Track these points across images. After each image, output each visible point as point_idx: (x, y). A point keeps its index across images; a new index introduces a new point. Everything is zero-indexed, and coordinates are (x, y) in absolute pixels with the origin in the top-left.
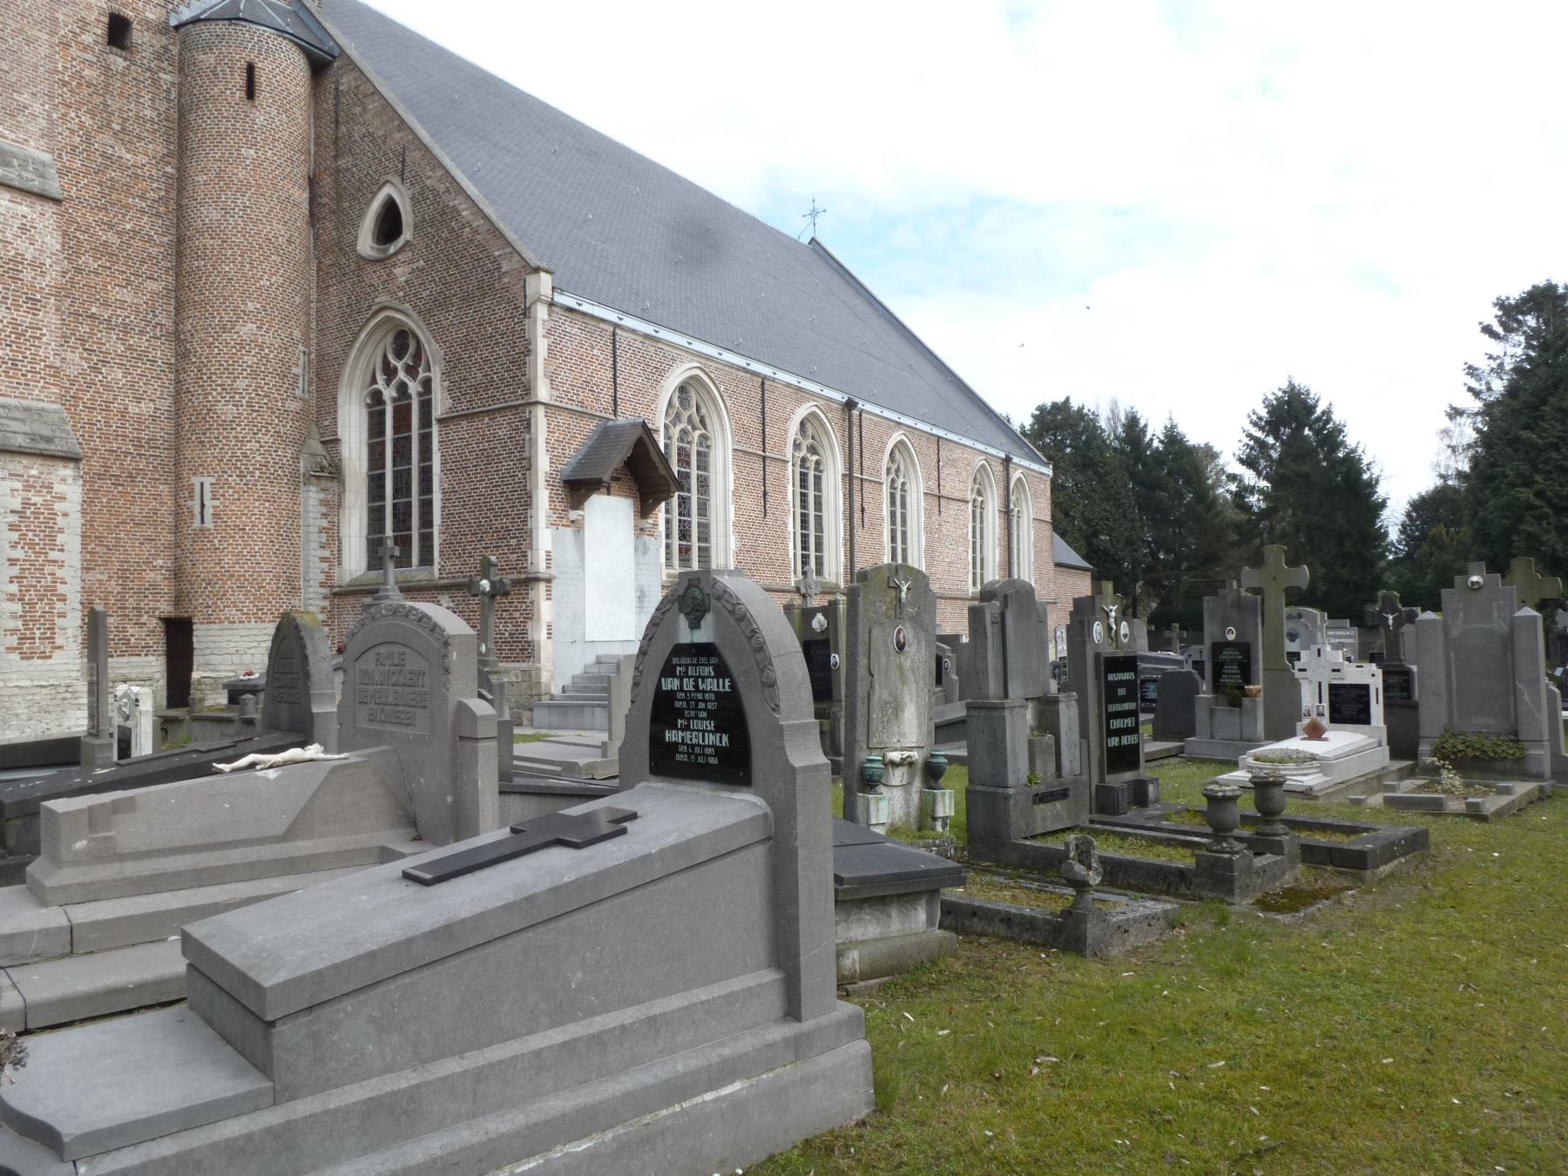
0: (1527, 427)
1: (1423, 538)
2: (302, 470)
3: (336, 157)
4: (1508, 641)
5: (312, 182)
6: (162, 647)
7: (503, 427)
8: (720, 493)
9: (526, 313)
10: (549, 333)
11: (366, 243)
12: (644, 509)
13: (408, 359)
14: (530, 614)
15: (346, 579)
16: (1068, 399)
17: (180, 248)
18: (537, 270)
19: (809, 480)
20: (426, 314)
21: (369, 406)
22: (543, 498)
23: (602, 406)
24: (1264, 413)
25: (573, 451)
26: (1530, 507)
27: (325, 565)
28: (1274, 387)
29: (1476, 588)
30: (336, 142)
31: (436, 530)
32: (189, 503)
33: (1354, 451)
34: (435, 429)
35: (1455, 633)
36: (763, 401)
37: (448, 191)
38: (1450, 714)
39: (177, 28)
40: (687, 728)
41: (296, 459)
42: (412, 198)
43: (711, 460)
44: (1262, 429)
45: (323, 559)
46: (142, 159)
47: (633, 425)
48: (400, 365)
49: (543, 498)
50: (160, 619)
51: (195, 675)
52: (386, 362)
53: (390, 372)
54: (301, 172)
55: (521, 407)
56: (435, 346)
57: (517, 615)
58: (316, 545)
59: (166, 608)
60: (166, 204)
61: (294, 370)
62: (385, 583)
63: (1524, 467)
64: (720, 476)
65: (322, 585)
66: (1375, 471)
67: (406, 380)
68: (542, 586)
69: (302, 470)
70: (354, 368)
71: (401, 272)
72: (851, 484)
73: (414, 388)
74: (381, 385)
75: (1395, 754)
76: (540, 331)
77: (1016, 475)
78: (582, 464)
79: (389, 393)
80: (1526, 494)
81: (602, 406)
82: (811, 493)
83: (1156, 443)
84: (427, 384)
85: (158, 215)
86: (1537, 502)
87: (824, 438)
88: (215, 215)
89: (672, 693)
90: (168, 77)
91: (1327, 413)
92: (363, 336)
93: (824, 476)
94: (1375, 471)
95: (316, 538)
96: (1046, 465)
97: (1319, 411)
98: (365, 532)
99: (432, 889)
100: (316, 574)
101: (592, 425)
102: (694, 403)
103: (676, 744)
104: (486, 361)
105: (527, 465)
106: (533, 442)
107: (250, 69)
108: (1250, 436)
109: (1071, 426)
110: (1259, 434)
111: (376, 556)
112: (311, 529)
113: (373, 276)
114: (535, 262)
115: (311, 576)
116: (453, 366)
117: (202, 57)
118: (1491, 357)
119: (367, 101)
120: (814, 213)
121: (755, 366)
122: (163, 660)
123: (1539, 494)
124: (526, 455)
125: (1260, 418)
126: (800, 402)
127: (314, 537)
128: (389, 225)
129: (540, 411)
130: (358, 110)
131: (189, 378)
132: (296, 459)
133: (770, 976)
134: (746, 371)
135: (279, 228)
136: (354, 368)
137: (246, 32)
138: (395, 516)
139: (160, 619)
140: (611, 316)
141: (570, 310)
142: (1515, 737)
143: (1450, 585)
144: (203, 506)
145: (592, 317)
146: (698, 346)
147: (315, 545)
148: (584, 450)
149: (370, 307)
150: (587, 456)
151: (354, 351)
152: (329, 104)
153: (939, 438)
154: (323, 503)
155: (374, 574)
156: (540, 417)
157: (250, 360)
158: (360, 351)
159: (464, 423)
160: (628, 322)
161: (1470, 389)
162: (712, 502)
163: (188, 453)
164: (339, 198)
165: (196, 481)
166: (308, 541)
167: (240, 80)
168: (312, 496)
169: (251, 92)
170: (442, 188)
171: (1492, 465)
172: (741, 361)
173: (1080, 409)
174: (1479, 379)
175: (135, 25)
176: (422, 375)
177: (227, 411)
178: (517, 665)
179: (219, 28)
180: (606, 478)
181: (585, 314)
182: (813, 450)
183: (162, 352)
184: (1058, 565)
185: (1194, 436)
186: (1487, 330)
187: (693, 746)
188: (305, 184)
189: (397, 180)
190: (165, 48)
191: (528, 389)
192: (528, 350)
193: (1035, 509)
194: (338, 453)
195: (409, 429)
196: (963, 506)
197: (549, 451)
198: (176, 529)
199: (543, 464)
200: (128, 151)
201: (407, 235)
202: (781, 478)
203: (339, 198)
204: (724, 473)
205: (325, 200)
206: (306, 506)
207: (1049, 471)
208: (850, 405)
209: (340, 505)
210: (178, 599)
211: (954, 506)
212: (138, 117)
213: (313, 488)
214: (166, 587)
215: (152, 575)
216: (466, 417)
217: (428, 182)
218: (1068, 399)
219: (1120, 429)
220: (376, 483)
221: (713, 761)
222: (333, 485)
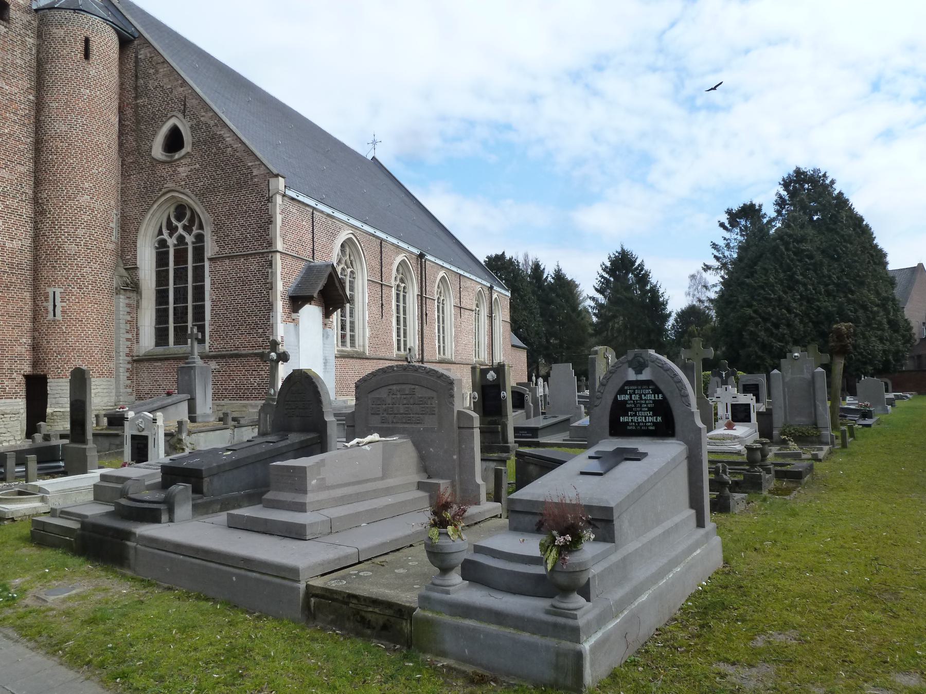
0: (747, 277)
1: (684, 332)
3: (136, 98)
4: (812, 382)
5: (121, 110)
6: (23, 393)
7: (254, 264)
8: (361, 304)
9: (270, 199)
10: (282, 212)
11: (158, 151)
12: (327, 315)
13: (185, 222)
15: (142, 352)
16: (504, 253)
17: (38, 146)
18: (277, 176)
19: (401, 297)
20: (201, 195)
21: (157, 248)
22: (280, 306)
23: (306, 255)
24: (608, 264)
26: (751, 318)
28: (614, 250)
29: (796, 359)
30: (136, 88)
31: (207, 323)
32: (45, 304)
33: (655, 286)
34: (207, 264)
35: (787, 379)
36: (381, 252)
37: (216, 125)
38: (786, 417)
39: (36, 11)
40: (635, 415)
42: (191, 127)
43: (356, 286)
44: (607, 273)
45: (128, 340)
46: (15, 90)
47: (327, 266)
48: (180, 225)
49: (280, 306)
50: (24, 375)
51: (49, 410)
52: (169, 222)
53: (172, 229)
54: (115, 104)
55: (264, 252)
56: (207, 215)
57: (263, 373)
58: (124, 331)
59: (27, 369)
60: (29, 118)
61: (111, 225)
62: (192, 353)
63: (748, 298)
64: (360, 295)
65: (127, 355)
66: (666, 297)
67: (184, 234)
70: (148, 225)
71: (183, 171)
72: (422, 300)
73: (189, 239)
74: (165, 235)
75: (762, 435)
76: (278, 211)
77: (495, 296)
78: (300, 285)
79: (171, 242)
80: (749, 311)
81: (306, 255)
82: (401, 305)
83: (549, 279)
84: (200, 238)
85: (24, 125)
86: (754, 315)
87: (408, 274)
88: (64, 128)
89: (625, 402)
90: (31, 40)
91: (641, 265)
92: (155, 206)
93: (407, 295)
94: (666, 297)
95: (124, 327)
96: (507, 290)
97: (637, 264)
99: (606, 476)
100: (123, 350)
101: (303, 265)
102: (347, 253)
103: (627, 423)
104: (242, 226)
105: (270, 287)
106: (274, 274)
107: (87, 41)
108: (602, 277)
109: (506, 268)
110: (606, 276)
111: (161, 336)
113: (163, 171)
114: (275, 172)
116: (218, 228)
117: (55, 30)
118: (725, 239)
119: (159, 66)
120: (374, 143)
121: (379, 234)
122: (24, 401)
123: (755, 312)
125: (606, 267)
126: (398, 254)
127: (123, 326)
128: (174, 141)
129: (278, 255)
130: (152, 71)
131: (45, 227)
133: (693, 512)
134: (374, 236)
135: (103, 139)
136: (148, 225)
137: (84, 18)
138: (175, 314)
139: (24, 375)
140: (312, 203)
141: (293, 199)
142: (815, 425)
143: (785, 357)
144: (55, 306)
145: (303, 203)
146: (353, 221)
148: (299, 279)
149: (160, 190)
150: (300, 283)
151: (149, 216)
152: (131, 65)
153: (461, 275)
154: (129, 305)
155: (160, 349)
156: (278, 260)
157: (86, 218)
158: (153, 215)
159: (227, 261)
160: (321, 207)
161: (715, 257)
162: (356, 309)
163: (44, 273)
164: (138, 122)
165: (53, 289)
167: (80, 47)
168: (122, 300)
169: (87, 55)
170: (212, 123)
171: (731, 296)
172: (371, 230)
173: (511, 259)
174: (718, 251)
175: (11, 6)
176: (195, 231)
177: (71, 248)
179: (68, 14)
180: (315, 295)
181: (299, 202)
182: (402, 281)
183: (26, 210)
184: (513, 346)
185: (570, 274)
186: (722, 225)
187: (639, 423)
188: (116, 111)
189: (180, 116)
190: (29, 22)
191: (270, 244)
192: (270, 221)
193: (503, 315)
195: (186, 262)
196: (471, 313)
197: (284, 279)
198: (35, 319)
199: (280, 286)
200: (7, 84)
201: (187, 148)
202: (389, 296)
203: (138, 122)
204: (362, 292)
205: (127, 123)
207: (509, 294)
208: (421, 256)
209: (138, 307)
210: (35, 364)
211: (467, 312)
212: (13, 64)
213: (122, 297)
214: (28, 356)
215: (19, 348)
216: (228, 257)
217: (202, 119)
218: (504, 253)
219: (529, 271)
220: (162, 297)
221: (651, 428)
222: (133, 295)
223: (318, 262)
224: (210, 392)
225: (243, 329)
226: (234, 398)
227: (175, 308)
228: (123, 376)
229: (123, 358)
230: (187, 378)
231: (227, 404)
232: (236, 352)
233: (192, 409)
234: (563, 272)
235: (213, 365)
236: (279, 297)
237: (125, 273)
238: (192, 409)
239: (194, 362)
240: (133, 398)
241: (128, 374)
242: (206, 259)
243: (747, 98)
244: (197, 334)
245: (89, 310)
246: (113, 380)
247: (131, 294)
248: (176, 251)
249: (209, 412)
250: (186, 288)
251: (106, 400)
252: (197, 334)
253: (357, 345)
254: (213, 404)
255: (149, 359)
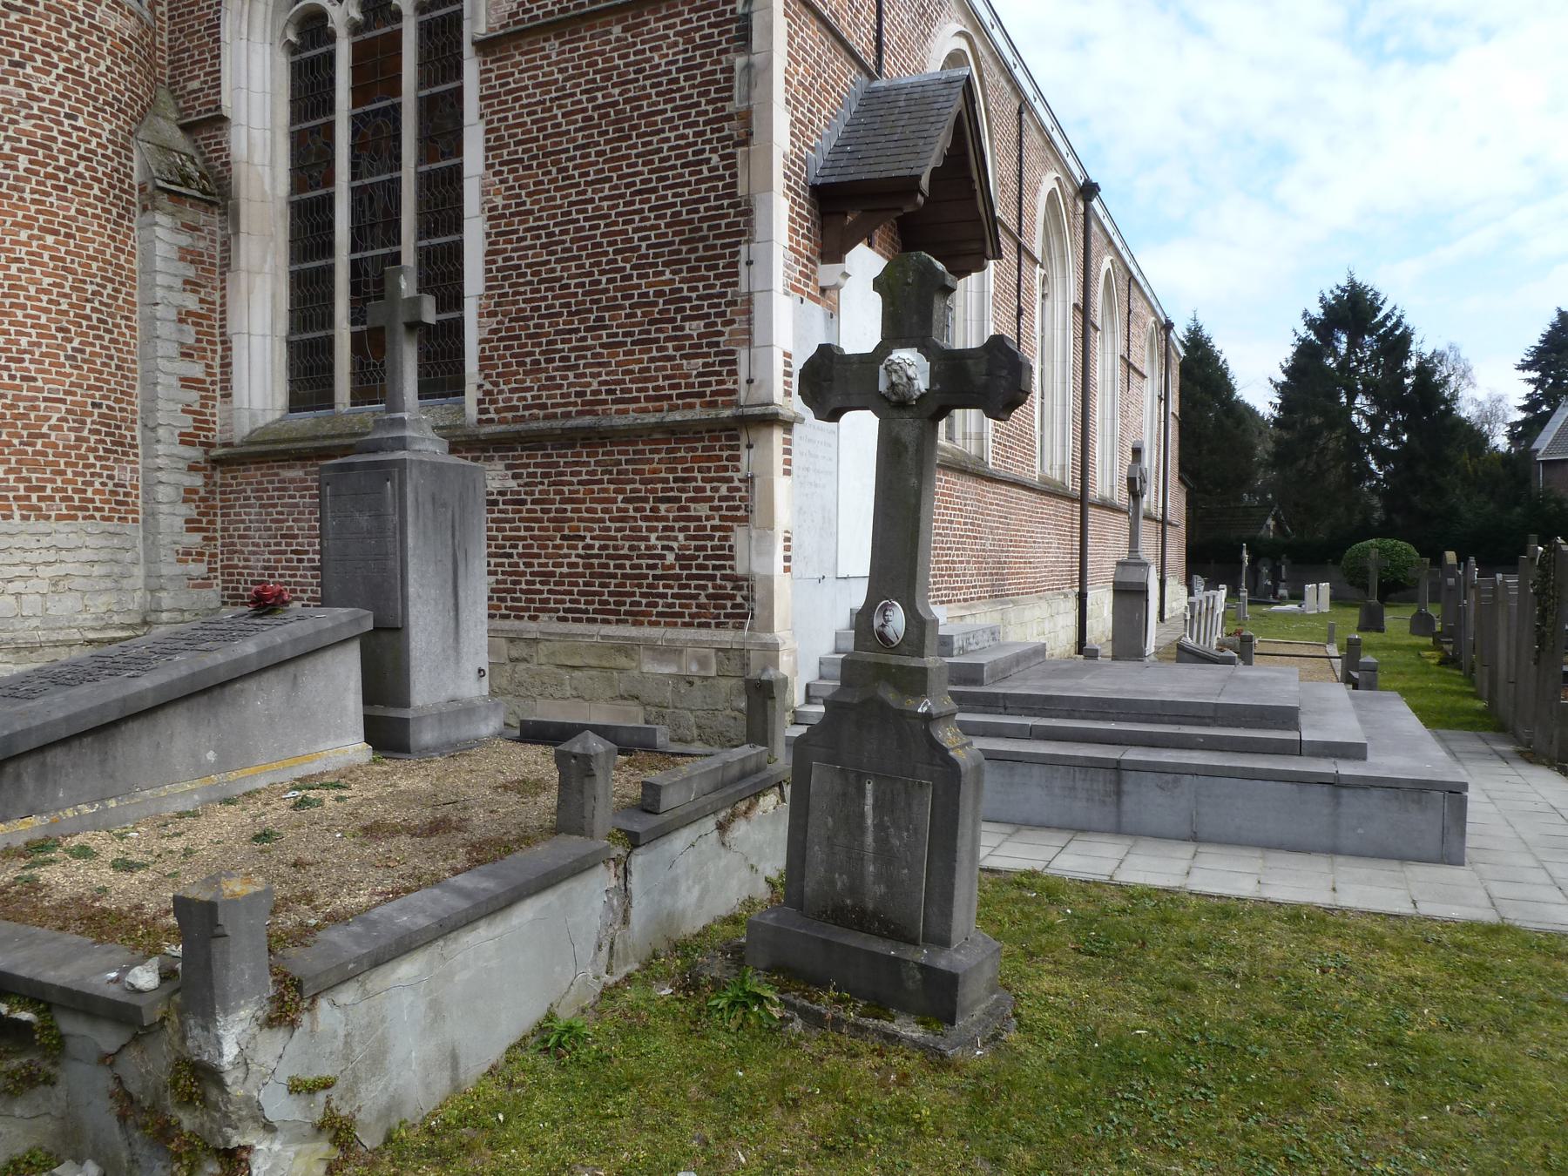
2: (137, 178)
14: (744, 506)
15: (243, 428)
21: (293, 49)
22: (781, 219)
25: (827, 132)
27: (193, 396)
28: (1331, 282)
41: (124, 149)
45: (188, 383)
49: (781, 219)
57: (702, 510)
58: (174, 350)
65: (186, 440)
68: (778, 435)
69: (137, 178)
97: (1381, 315)
98: (283, 326)
100: (172, 413)
106: (758, 74)
112: (160, 311)
115: (161, 418)
124: (730, 108)
127: (166, 329)
132: (124, 149)
147: (168, 348)
154: (187, 255)
155: (306, 419)
159: (552, 47)
166: (153, 338)
168: (162, 237)
178: (704, 634)
194: (222, 149)
197: (793, 124)
206: (148, 258)
209: (227, 264)
213: (160, 218)
223: (896, 72)
224: (478, 586)
225: (615, 323)
226: (574, 614)
227: (354, 264)
228: (173, 518)
229: (168, 448)
230: (364, 520)
231: (548, 637)
232: (587, 420)
233: (384, 683)
234: (1205, 332)
235: (495, 476)
236: (779, 182)
237: (179, 140)
238: (384, 683)
239: (401, 444)
240: (212, 596)
241: (190, 511)
242: (468, 49)
243: (1487, 34)
244: (415, 303)
245: (21, 252)
246: (135, 532)
247: (202, 218)
248: (360, 53)
249: (474, 689)
250: (394, 187)
251: (100, 604)
252: (415, 303)
253: (958, 435)
254: (493, 633)
255: (263, 454)
